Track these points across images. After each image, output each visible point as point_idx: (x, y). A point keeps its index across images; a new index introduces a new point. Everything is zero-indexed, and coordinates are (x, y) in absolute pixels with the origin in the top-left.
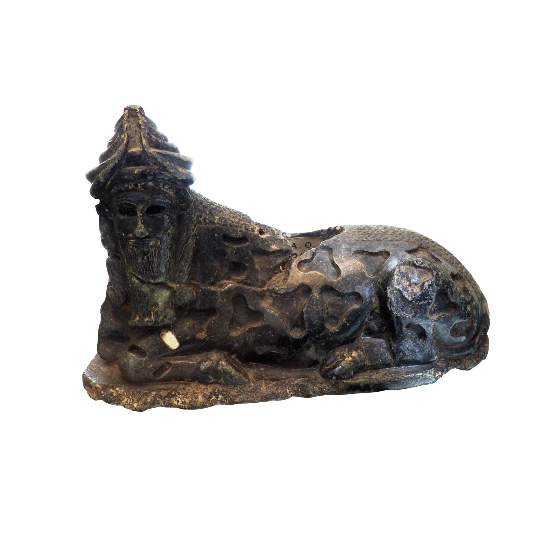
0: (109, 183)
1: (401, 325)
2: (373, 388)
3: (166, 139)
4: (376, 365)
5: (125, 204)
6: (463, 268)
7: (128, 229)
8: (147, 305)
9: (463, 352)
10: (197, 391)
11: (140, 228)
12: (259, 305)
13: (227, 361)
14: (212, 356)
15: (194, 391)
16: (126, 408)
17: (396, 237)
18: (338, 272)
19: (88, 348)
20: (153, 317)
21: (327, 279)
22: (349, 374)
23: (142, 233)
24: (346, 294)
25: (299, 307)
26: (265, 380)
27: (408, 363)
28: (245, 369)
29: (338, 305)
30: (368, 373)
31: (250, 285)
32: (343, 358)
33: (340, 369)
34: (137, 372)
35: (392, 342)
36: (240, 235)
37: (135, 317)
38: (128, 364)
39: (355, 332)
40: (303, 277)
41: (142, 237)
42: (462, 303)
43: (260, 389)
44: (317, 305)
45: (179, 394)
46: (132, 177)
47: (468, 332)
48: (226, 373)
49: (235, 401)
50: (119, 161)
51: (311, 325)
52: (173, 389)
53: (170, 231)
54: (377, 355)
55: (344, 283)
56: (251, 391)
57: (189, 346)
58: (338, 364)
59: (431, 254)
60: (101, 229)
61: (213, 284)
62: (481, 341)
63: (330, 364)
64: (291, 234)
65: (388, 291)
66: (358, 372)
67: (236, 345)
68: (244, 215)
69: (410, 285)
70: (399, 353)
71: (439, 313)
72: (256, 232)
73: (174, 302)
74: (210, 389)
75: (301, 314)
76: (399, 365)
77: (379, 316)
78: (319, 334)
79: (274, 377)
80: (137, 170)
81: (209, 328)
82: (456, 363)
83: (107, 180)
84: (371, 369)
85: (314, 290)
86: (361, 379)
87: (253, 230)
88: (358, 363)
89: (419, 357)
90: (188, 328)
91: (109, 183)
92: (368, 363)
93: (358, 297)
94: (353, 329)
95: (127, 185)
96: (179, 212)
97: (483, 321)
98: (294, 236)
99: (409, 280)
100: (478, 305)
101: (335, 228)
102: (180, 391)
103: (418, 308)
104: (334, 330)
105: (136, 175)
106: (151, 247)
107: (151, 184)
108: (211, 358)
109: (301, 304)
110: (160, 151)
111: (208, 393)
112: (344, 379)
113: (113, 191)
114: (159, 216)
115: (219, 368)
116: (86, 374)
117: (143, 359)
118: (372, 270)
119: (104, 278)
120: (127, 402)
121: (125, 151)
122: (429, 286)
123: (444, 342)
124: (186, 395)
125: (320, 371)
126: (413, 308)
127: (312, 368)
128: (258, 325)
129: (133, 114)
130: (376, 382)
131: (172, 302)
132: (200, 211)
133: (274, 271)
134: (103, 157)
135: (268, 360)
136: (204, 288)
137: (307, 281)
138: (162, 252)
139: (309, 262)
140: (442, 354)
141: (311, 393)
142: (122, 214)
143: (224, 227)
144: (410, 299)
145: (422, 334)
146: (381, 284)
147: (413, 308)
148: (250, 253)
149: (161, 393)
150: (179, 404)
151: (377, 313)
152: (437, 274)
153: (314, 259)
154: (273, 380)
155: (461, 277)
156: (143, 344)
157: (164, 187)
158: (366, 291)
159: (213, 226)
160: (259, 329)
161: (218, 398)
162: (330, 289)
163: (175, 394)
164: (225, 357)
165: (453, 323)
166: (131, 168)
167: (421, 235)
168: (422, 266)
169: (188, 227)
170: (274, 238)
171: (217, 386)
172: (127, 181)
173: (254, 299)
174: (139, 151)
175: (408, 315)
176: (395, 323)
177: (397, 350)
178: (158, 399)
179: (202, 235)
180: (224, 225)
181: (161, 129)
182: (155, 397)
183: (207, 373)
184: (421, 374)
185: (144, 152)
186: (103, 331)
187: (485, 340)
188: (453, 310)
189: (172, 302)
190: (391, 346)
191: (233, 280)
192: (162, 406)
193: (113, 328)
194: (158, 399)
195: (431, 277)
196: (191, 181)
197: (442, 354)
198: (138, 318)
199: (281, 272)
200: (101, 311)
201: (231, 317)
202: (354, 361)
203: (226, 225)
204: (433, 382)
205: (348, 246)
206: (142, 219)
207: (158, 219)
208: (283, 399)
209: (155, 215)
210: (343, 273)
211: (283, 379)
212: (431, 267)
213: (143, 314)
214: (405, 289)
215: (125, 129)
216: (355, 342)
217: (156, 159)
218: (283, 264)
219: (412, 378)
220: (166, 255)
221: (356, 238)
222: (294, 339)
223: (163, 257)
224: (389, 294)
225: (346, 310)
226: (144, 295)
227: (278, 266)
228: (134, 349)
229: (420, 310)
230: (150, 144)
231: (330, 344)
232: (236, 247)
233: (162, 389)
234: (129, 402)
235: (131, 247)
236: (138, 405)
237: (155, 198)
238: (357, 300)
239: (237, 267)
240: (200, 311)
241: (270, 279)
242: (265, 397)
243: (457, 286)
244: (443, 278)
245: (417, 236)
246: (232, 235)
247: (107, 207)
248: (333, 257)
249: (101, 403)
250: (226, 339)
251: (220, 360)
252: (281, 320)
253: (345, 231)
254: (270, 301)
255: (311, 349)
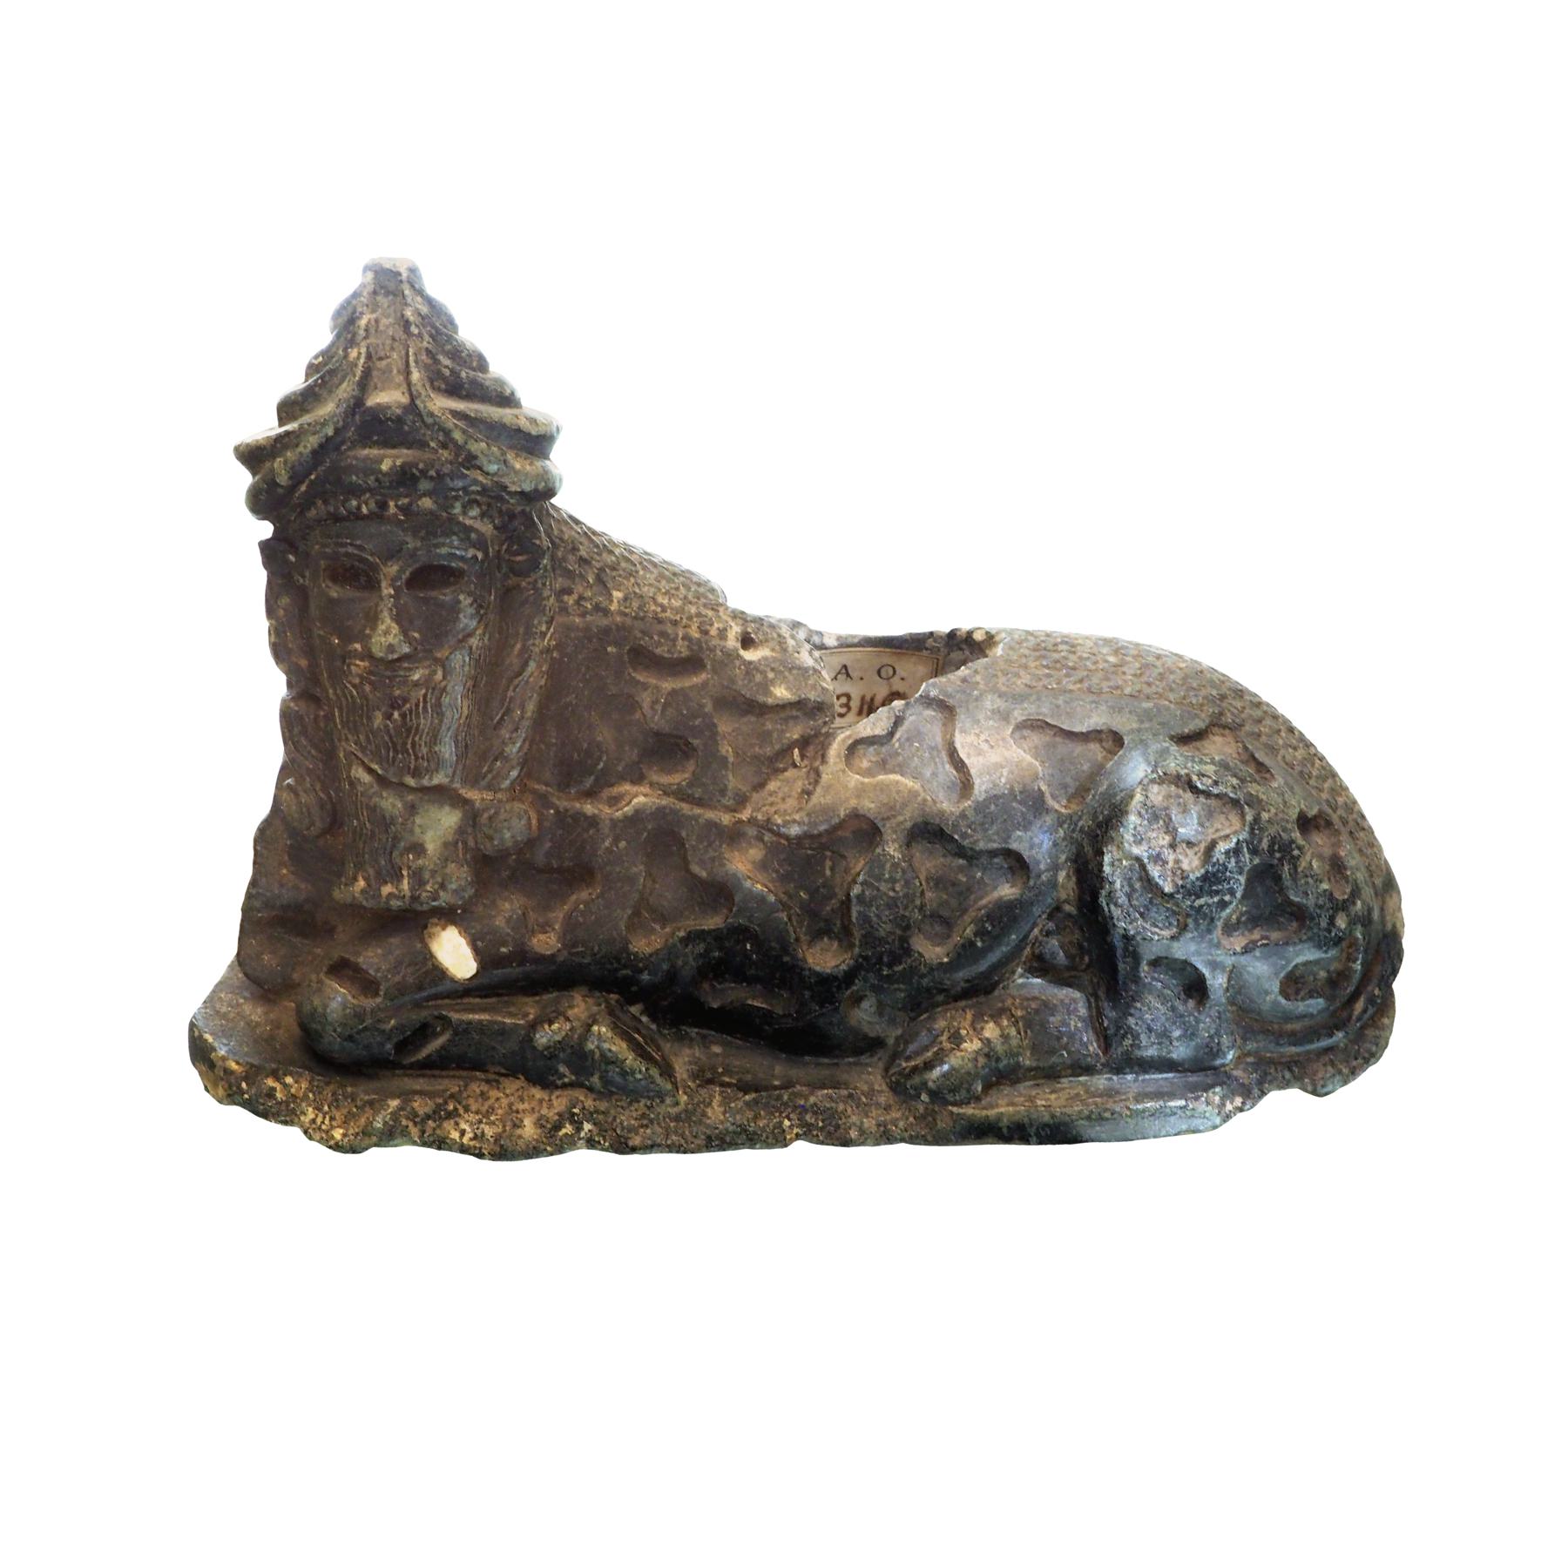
0: (303, 488)
1: (1136, 958)
2: (1038, 1135)
3: (482, 365)
4: (1051, 1067)
5: (347, 555)
6: (1340, 789)
7: (351, 627)
8: (389, 845)
9: (1311, 1042)
10: (521, 1107)
11: (386, 633)
12: (723, 865)
13: (615, 1027)
14: (571, 1007)
15: (510, 1105)
16: (311, 1138)
17: (1149, 684)
18: (966, 785)
19: (207, 944)
20: (405, 885)
21: (930, 802)
22: (968, 1091)
23: (391, 648)
24: (981, 852)
25: (838, 880)
26: (723, 1085)
27: (1146, 1066)
28: (667, 1047)
29: (954, 884)
30: (1025, 1087)
31: (699, 803)
32: (956, 1039)
33: (944, 1075)
34: (350, 1038)
35: (1106, 1005)
36: (682, 649)
37: (355, 879)
38: (324, 1015)
39: (995, 968)
40: (861, 791)
41: (390, 657)
42: (1320, 907)
43: (704, 1114)
44: (893, 881)
45: (467, 1109)
46: (371, 481)
47: (1335, 981)
48: (609, 1060)
49: (631, 1143)
50: (337, 431)
51: (870, 939)
52: (452, 1096)
53: (474, 642)
54: (1059, 1039)
55: (980, 818)
56: (677, 1118)
57: (508, 973)
58: (939, 1058)
59: (1246, 748)
60: (270, 612)
61: (590, 794)
62: (1371, 1011)
63: (918, 1053)
64: (839, 638)
65: (1107, 859)
66: (998, 1083)
67: (645, 977)
68: (699, 585)
69: (1173, 846)
70: (1124, 1036)
71: (1251, 931)
72: (732, 642)
73: (471, 843)
74: (560, 1102)
75: (842, 902)
76: (1118, 1071)
77: (1075, 923)
78: (890, 966)
79: (749, 1077)
80: (389, 461)
81: (570, 926)
82: (1288, 1075)
83: (297, 477)
84: (1034, 1078)
85: (888, 834)
86: (1005, 1105)
87: (722, 634)
88: (998, 1060)
89: (1180, 1052)
90: (508, 921)
91: (303, 488)
92: (1027, 1061)
93: (1017, 864)
94: (993, 957)
95: (354, 503)
96: (506, 577)
97: (1385, 951)
98: (845, 644)
99: (1170, 829)
100: (1370, 910)
101: (970, 633)
102: (471, 1101)
103: (1188, 915)
104: (938, 957)
105: (385, 475)
106: (416, 684)
107: (427, 503)
108: (570, 1013)
109: (847, 870)
110: (460, 406)
111: (552, 1114)
112: (955, 1104)
113: (312, 513)
114: (446, 596)
115: (591, 1046)
116: (200, 1024)
117: (370, 1003)
118: (1065, 787)
119: (271, 751)
120: (314, 1121)
121: (358, 403)
122: (1227, 853)
123: (1259, 1014)
124: (487, 1115)
125: (887, 1070)
126: (1174, 913)
127: (864, 1059)
128: (713, 922)
129: (390, 284)
130: (1047, 1118)
131: (465, 843)
132: (570, 574)
133: (775, 763)
134: (289, 408)
135: (737, 1025)
136: (563, 804)
137: (869, 806)
138: (446, 700)
139: (882, 745)
140: (1251, 1046)
141: (853, 1134)
142: (335, 578)
143: (638, 624)
144: (1168, 889)
145: (1196, 988)
146: (1087, 834)
147: (1174, 913)
148: (709, 708)
149: (416, 1105)
150: (465, 1140)
151: (1069, 915)
152: (1257, 819)
153: (897, 736)
154: (744, 1088)
155: (1329, 824)
156: (372, 958)
157: (464, 513)
158: (1040, 844)
159: (605, 622)
160: (717, 936)
161: (579, 1129)
162: (935, 834)
163: (456, 1109)
164: (611, 1013)
165: (1288, 962)
166: (375, 452)
167: (1225, 679)
168: (1216, 791)
169: (528, 627)
170: (783, 663)
171: (580, 1094)
172: (355, 491)
173: (710, 845)
174: (399, 406)
175: (1156, 936)
176: (1119, 952)
177: (1118, 1028)
178: (404, 1122)
179: (569, 650)
180: (635, 618)
181: (471, 332)
182: (395, 1116)
183: (553, 1057)
184: (1182, 1103)
185: (412, 408)
186: (257, 904)
187: (1384, 1006)
188: (1295, 924)
189: (465, 843)
190: (1100, 1014)
191: (651, 785)
192: (415, 1143)
193: (287, 896)
194: (404, 1122)
195: (1237, 824)
196: (550, 493)
197: (1251, 1046)
198: (362, 883)
199: (795, 766)
200: (256, 841)
201: (636, 896)
202: (989, 1053)
203: (642, 619)
204: (1215, 1127)
205: (1000, 703)
206: (395, 606)
207: (442, 605)
208: (768, 1145)
209: (434, 594)
210: (981, 787)
211: (776, 1088)
212: (1240, 795)
213: (378, 873)
214: (1157, 858)
215: (362, 333)
216: (996, 993)
217: (447, 433)
218: (804, 743)
219: (1153, 1114)
220: (457, 702)
221: (1026, 679)
222: (818, 974)
223: (448, 714)
224: (1107, 869)
225: (975, 902)
226: (385, 822)
227: (787, 750)
228: (342, 969)
229: (1196, 921)
230: (432, 381)
231: (925, 997)
232: (668, 685)
233: (421, 1093)
234: (319, 1120)
235: (357, 681)
236: (344, 1135)
237: (437, 546)
238: (1013, 873)
239: (668, 747)
240: (549, 870)
241: (760, 786)
242: (717, 1137)
243: (1313, 853)
244: (1272, 831)
245: (1213, 684)
246: (658, 651)
247: (293, 547)
248: (953, 735)
249: (239, 1115)
250: (618, 960)
251: (595, 1022)
252: (784, 916)
253: (999, 651)
254: (756, 853)
255: (865, 1004)
